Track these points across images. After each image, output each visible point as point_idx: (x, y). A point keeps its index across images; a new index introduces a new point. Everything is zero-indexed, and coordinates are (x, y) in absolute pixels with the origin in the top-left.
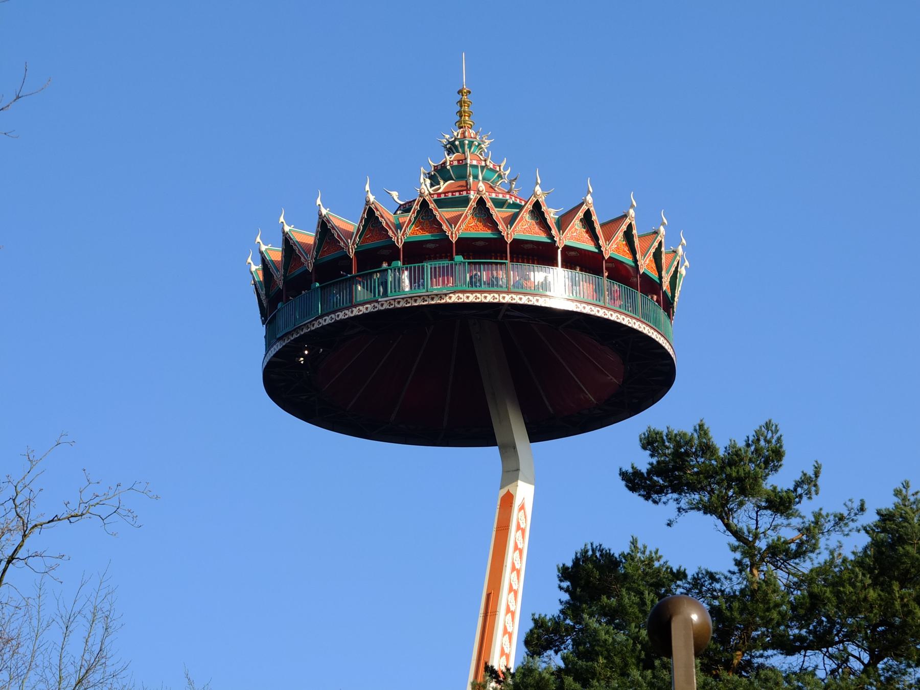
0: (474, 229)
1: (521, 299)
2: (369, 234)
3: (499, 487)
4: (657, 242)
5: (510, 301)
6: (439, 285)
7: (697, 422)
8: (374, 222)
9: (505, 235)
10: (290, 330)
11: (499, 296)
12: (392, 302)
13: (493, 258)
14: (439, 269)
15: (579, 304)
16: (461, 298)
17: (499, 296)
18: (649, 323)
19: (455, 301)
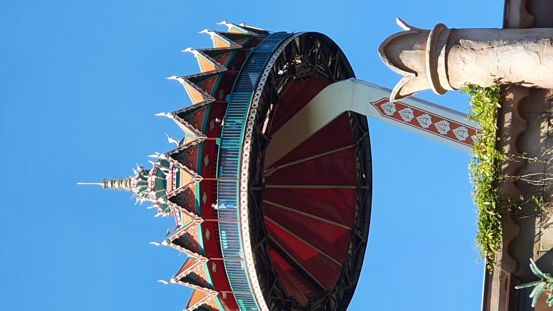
0: (210, 90)
1: (246, 155)
2: (201, 279)
3: (535, 308)
4: (176, 247)
5: (247, 170)
6: (237, 224)
7: (417, 77)
8: (192, 276)
9: (209, 102)
10: (269, 144)
11: (243, 191)
12: (252, 110)
13: (216, 193)
14: (231, 114)
15: (248, 157)
16: (244, 207)
17: (243, 191)
18: (265, 63)
19: (246, 184)
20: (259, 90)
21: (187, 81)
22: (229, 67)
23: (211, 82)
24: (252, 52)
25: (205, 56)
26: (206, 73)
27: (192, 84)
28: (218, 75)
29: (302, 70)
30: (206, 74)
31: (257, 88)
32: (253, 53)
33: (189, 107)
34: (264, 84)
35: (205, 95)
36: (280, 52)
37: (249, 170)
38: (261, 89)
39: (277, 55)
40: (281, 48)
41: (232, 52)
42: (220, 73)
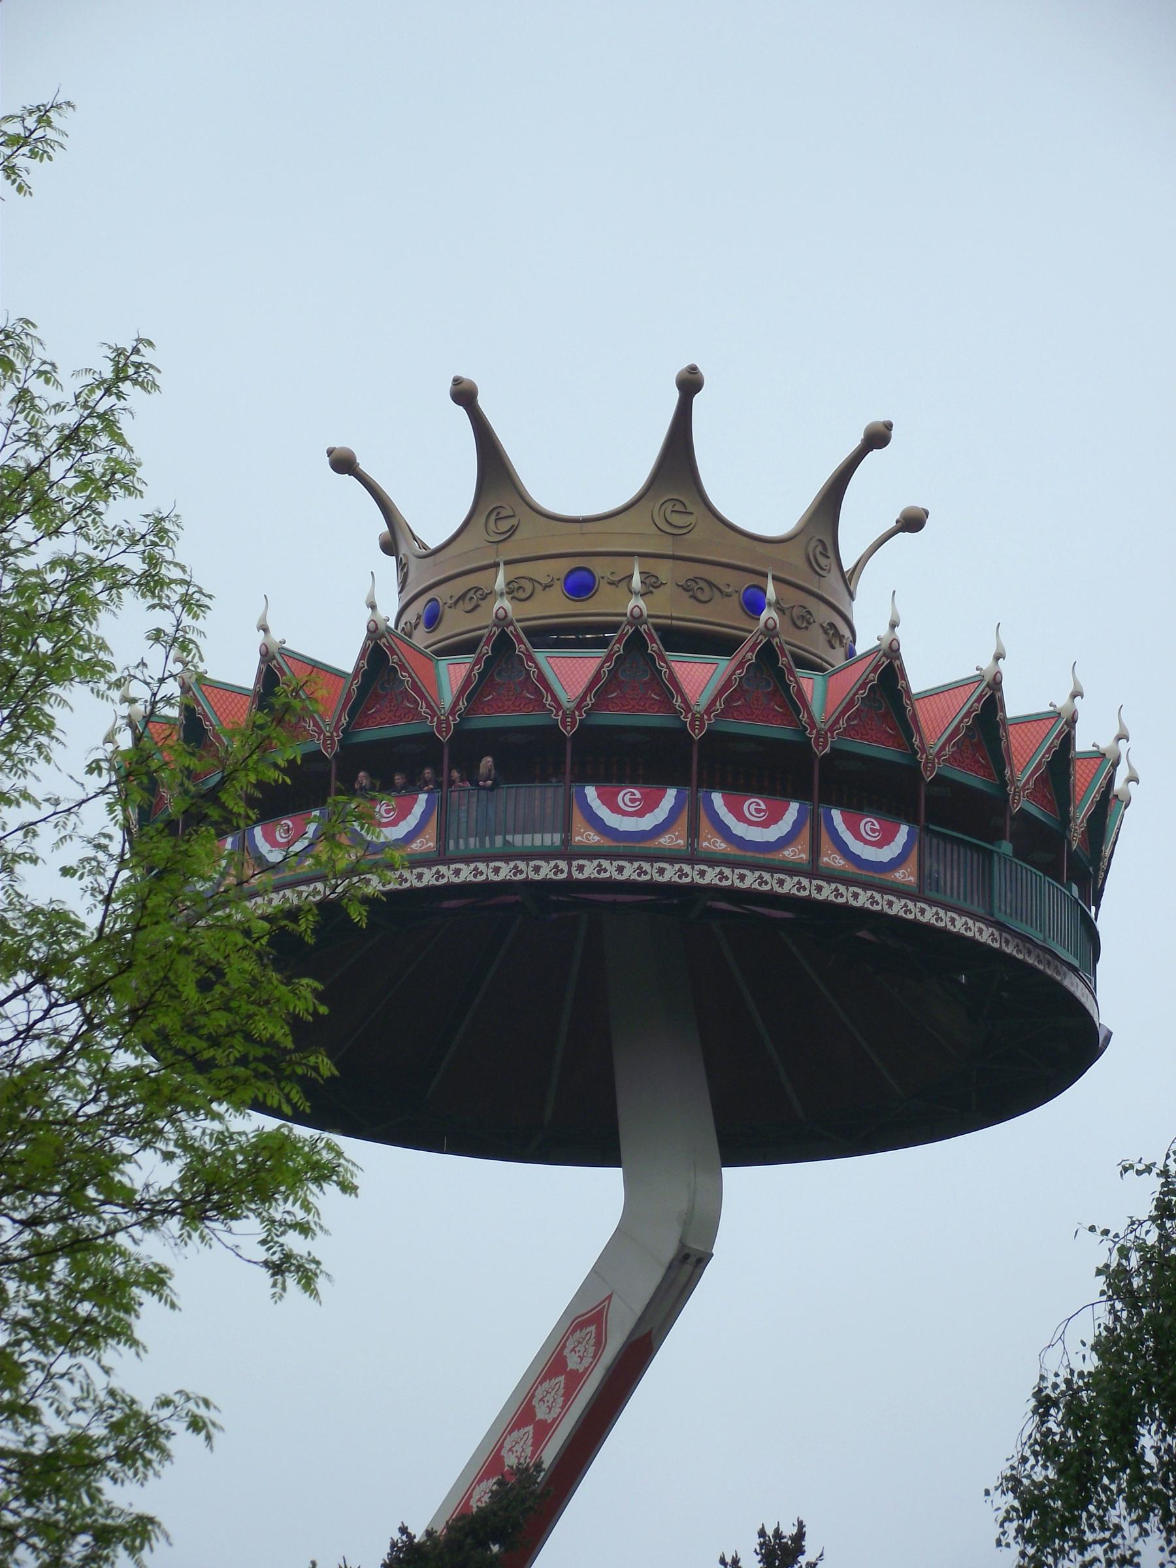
20: (906, 906)
21: (884, 659)
22: (939, 780)
23: (979, 762)
24: (992, 852)
25: (1056, 741)
26: (914, 716)
27: (874, 677)
28: (910, 752)
29: (139, 1009)
30: (1003, 745)
31: (844, 885)
32: (989, 854)
33: (852, 699)
34: (892, 912)
35: (945, 750)
36: (1005, 948)
37: (434, 887)
38: (939, 919)
39: (994, 940)
40: (1021, 947)
41: (998, 783)
42: (916, 759)
